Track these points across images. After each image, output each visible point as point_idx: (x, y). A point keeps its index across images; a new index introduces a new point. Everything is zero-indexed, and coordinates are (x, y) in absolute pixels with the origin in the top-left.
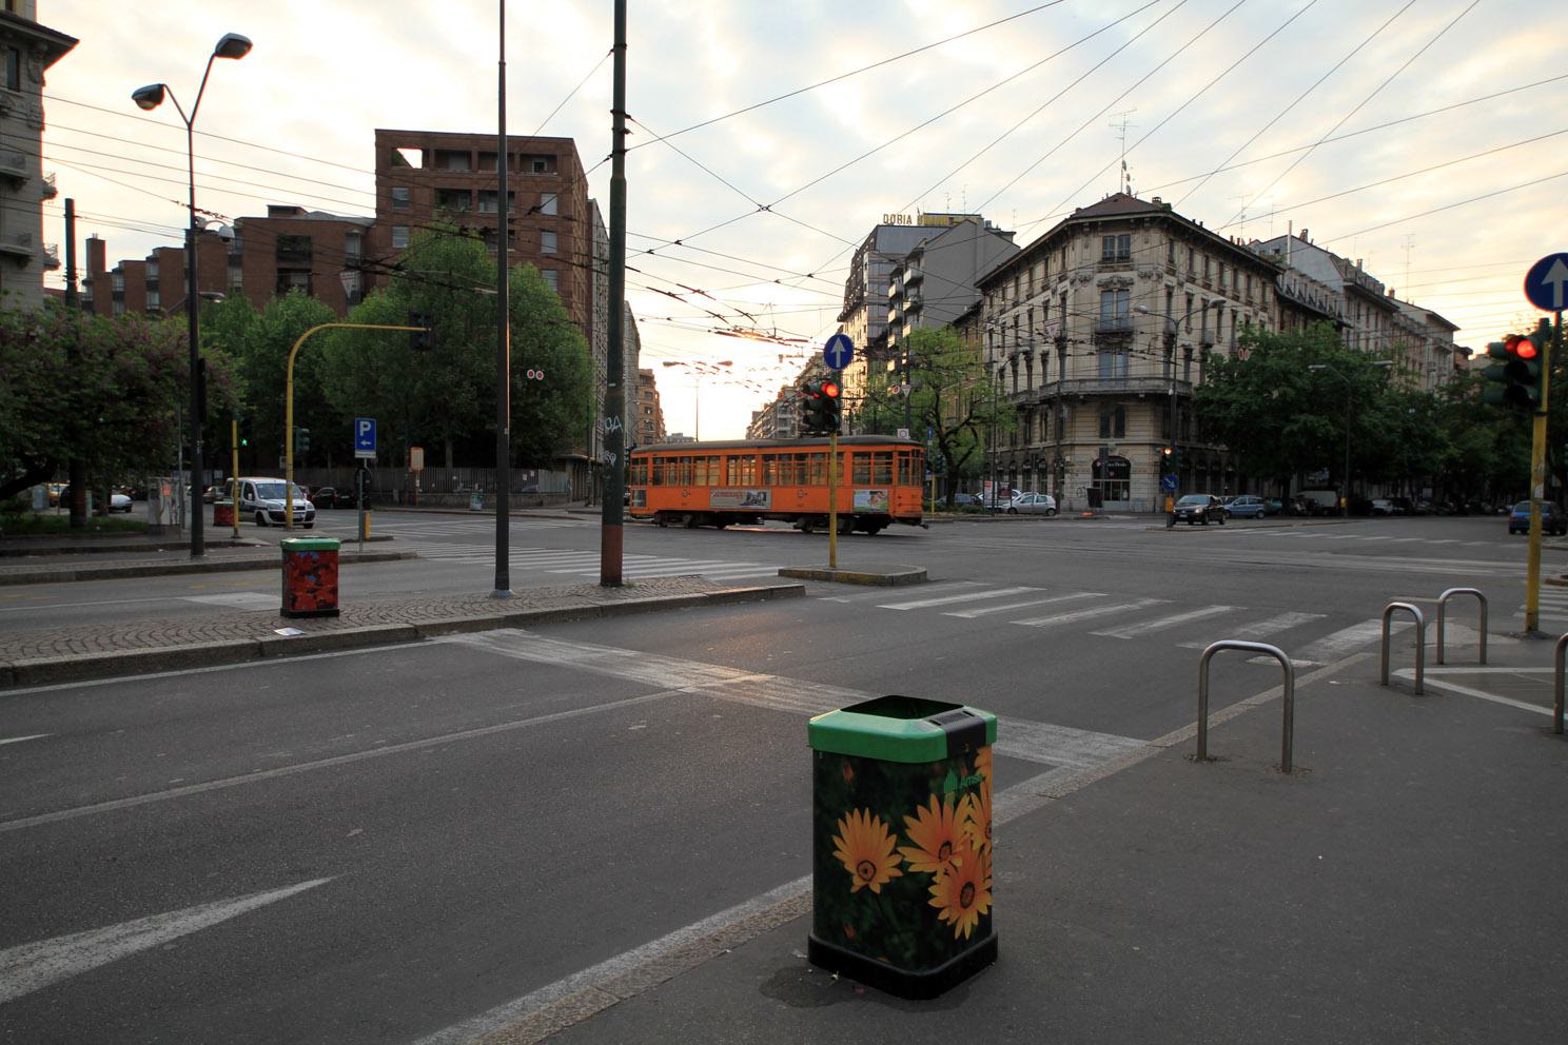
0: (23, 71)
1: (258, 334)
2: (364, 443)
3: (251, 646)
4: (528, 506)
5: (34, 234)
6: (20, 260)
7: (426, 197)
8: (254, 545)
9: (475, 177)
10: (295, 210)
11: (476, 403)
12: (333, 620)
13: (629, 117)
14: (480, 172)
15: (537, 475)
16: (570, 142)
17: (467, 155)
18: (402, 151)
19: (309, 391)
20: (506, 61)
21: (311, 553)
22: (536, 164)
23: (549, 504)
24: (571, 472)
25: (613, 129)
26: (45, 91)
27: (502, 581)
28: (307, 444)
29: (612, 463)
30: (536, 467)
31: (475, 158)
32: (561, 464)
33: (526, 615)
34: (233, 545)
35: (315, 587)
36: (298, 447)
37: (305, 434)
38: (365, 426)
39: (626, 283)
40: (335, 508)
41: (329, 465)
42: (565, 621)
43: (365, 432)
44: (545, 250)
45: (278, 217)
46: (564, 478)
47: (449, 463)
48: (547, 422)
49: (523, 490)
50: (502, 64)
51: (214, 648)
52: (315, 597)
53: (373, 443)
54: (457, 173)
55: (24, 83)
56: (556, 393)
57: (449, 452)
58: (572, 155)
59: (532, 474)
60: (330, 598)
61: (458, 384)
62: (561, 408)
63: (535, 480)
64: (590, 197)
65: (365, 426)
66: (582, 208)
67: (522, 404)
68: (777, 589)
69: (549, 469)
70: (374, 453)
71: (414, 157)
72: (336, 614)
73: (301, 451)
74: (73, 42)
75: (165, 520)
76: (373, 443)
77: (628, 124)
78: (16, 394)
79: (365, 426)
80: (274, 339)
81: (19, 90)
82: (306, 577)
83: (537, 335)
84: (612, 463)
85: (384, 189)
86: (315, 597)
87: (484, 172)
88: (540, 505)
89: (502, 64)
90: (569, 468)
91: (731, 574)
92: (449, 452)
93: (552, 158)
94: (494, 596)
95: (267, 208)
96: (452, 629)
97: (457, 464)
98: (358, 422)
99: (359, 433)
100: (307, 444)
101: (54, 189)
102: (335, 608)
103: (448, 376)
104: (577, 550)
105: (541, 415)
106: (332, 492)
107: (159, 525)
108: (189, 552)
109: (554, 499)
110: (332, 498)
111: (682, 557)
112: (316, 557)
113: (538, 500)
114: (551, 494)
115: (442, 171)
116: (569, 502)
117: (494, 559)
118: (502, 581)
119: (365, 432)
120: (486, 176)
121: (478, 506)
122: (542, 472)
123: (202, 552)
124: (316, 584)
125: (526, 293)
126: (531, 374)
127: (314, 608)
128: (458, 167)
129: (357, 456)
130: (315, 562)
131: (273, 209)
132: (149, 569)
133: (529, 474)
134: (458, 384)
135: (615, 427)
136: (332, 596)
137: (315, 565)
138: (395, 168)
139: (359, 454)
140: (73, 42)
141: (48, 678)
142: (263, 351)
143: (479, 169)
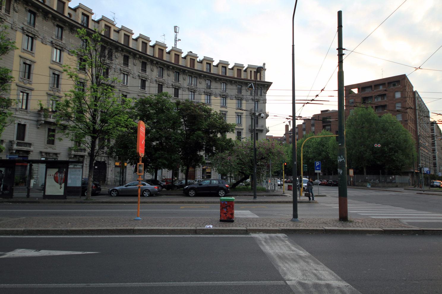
0: (263, 92)
1: (314, 142)
2: (317, 168)
3: (193, 230)
4: (392, 187)
5: (264, 125)
6: (261, 131)
7: (359, 100)
8: (287, 196)
9: (373, 92)
10: (327, 111)
11: (372, 156)
12: (231, 224)
13: (344, 49)
14: (375, 90)
15: (395, 177)
16: (405, 74)
17: (371, 87)
18: (352, 90)
19: (326, 155)
20: (294, 44)
21: (225, 202)
22: (393, 84)
23: (231, 192)
24: (411, 176)
25: (338, 55)
26: (267, 95)
27: (295, 215)
28: (306, 169)
29: (341, 173)
30: (395, 175)
31: (373, 87)
32: (406, 174)
33: (301, 230)
34: (282, 196)
35: (226, 212)
36: (304, 170)
37: (306, 166)
38: (318, 163)
39: (337, 105)
40: (333, 186)
41: (333, 174)
42: (308, 233)
43: (318, 165)
44: (397, 108)
45: (322, 113)
46: (408, 178)
47: (365, 174)
48: (397, 160)
49: (393, 182)
50: (293, 46)
51: (183, 229)
52: (226, 216)
53: (320, 168)
54: (368, 93)
55: (263, 94)
56: (400, 151)
57: (365, 170)
58: (405, 79)
59: (393, 177)
60: (230, 216)
61: (366, 151)
62: (402, 156)
63: (394, 179)
64: (414, 90)
65: (318, 164)
66: (411, 95)
67: (387, 155)
68: (426, 230)
69: (400, 175)
70: (320, 171)
71: (355, 91)
72: (233, 221)
73: (305, 171)
74: (272, 83)
75: (269, 189)
76: (320, 168)
77: (344, 52)
78: (237, 159)
79: (318, 164)
80: (318, 143)
81: (262, 96)
82: (223, 209)
83: (391, 134)
84: (341, 173)
85: (347, 101)
86: (226, 216)
87: (376, 90)
88: (397, 186)
89: (293, 46)
90: (410, 175)
91: (423, 219)
92: (365, 170)
93: (398, 82)
94: (292, 220)
95: (320, 112)
96: (260, 232)
97: (367, 174)
98: (316, 162)
99: (316, 165)
100: (306, 169)
101: (268, 115)
102: (232, 219)
103: (362, 148)
104: (377, 204)
105: (395, 158)
106: (332, 182)
107: (268, 190)
108: (253, 197)
109: (402, 185)
110: (332, 183)
111: (412, 209)
112: (226, 203)
113: (396, 185)
114: (402, 183)
115: (363, 93)
116: (410, 185)
117: (338, 205)
118: (295, 215)
119: (318, 165)
120: (376, 92)
121: (370, 187)
122: (397, 176)
123: (256, 198)
124: (226, 211)
125: (387, 122)
126: (376, 145)
127: (226, 219)
128: (368, 91)
129: (315, 172)
130: (226, 205)
131: (322, 111)
132: (240, 201)
133: (392, 177)
134: (366, 151)
135: (341, 160)
136: (231, 216)
137: (226, 206)
138: (350, 95)
139: (316, 171)
140: (272, 83)
141: (140, 233)
142: (315, 146)
143: (374, 89)
